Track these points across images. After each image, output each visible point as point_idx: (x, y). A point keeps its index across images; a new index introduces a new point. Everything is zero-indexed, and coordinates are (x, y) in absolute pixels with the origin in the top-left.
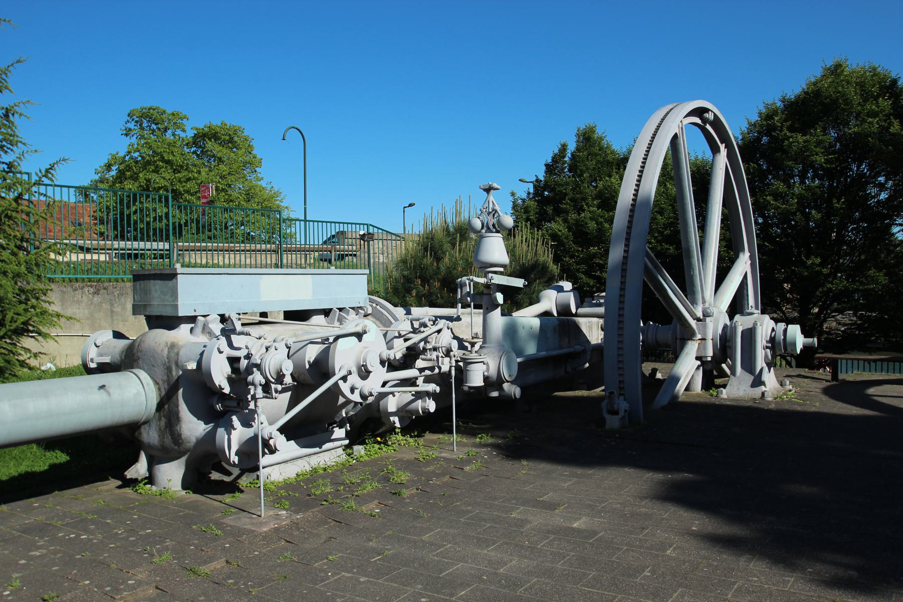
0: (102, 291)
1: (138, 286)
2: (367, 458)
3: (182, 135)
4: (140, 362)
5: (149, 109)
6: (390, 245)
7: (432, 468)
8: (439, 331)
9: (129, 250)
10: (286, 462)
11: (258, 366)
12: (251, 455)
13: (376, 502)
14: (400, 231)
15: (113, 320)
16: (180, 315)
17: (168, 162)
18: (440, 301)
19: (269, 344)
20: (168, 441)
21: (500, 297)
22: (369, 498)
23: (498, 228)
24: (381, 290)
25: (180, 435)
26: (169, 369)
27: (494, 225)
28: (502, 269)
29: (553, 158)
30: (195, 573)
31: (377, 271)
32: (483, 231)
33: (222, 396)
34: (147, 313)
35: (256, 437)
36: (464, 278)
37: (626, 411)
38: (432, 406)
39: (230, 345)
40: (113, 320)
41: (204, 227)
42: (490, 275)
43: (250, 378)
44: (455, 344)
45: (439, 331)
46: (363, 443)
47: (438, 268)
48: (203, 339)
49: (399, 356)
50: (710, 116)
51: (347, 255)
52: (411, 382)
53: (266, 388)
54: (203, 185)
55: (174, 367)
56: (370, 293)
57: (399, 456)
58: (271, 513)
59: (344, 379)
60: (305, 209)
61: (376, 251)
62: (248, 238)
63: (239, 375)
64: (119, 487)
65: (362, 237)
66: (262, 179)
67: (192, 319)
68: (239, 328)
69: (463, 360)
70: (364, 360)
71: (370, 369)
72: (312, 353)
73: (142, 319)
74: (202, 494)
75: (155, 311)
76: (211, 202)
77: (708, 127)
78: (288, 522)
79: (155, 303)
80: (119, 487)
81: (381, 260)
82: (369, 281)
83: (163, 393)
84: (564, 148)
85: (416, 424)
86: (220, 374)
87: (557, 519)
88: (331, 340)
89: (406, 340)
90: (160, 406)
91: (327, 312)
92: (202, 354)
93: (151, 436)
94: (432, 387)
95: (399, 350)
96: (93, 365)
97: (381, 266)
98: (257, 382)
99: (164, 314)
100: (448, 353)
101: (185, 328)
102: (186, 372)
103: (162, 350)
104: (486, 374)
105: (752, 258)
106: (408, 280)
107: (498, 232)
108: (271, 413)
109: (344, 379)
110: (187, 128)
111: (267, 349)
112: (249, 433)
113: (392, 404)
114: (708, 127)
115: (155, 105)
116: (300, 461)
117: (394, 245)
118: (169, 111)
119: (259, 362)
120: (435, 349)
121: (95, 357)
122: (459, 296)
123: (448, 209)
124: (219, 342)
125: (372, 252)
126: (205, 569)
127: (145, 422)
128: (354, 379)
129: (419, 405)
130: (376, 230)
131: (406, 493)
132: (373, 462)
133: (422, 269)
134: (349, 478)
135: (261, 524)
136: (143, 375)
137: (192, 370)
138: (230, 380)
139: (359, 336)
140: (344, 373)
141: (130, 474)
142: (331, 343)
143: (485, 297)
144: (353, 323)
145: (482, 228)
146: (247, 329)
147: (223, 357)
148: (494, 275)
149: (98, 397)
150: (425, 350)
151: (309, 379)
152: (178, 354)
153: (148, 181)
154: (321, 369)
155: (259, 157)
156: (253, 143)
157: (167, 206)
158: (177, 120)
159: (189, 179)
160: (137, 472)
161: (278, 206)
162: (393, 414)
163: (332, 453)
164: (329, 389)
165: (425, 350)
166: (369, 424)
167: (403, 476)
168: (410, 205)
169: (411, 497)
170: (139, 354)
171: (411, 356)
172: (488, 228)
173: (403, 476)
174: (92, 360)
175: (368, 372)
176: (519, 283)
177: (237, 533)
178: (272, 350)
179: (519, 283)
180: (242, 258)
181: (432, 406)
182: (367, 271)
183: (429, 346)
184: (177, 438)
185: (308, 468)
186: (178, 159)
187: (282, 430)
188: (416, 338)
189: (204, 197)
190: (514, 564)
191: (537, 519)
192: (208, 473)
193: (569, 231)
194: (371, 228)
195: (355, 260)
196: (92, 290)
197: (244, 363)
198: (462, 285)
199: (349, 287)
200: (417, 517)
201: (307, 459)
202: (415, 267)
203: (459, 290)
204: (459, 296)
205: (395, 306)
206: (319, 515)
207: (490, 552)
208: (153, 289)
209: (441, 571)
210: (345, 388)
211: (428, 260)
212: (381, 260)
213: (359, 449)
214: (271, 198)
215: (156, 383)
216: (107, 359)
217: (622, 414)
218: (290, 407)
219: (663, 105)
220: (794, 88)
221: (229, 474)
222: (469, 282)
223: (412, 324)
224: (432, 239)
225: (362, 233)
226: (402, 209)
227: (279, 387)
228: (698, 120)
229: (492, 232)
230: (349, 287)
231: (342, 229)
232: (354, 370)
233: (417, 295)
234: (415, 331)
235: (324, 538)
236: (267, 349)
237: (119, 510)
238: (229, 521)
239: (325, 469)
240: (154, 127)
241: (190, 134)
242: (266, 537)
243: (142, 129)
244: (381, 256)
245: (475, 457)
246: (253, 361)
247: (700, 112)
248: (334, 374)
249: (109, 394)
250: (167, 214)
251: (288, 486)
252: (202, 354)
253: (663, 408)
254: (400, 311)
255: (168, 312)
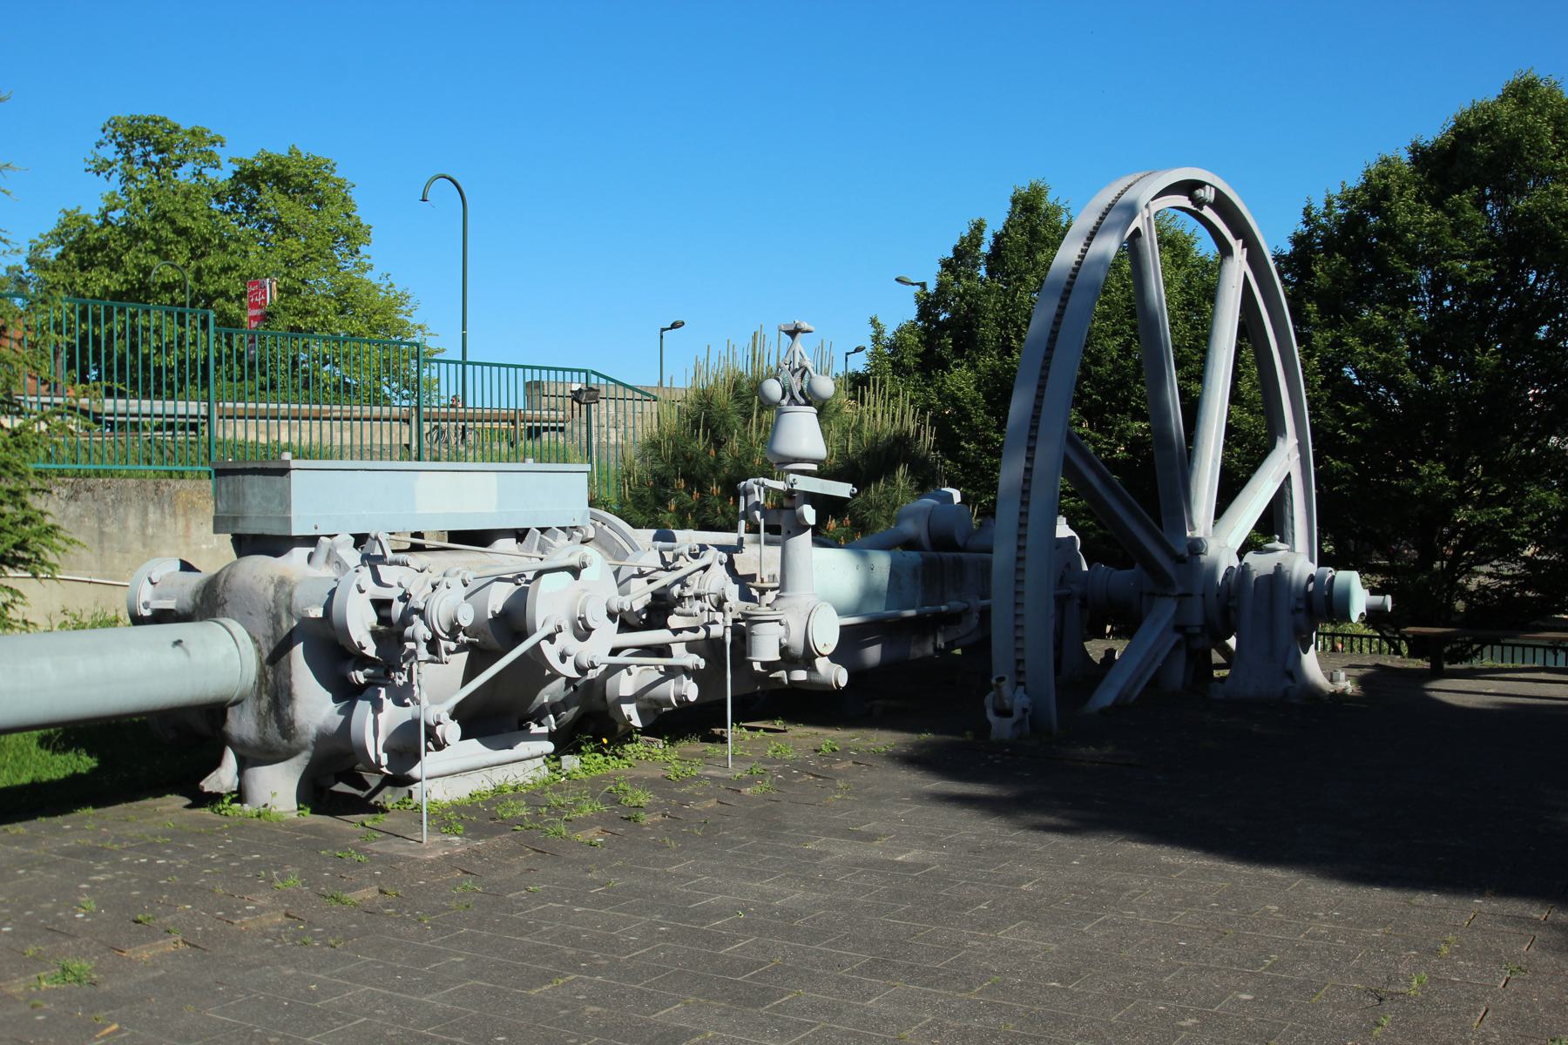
0: (84, 494)
1: (223, 488)
2: (583, 775)
3: (211, 174)
4: (228, 607)
5: (146, 121)
6: (629, 410)
7: (688, 789)
8: (706, 568)
9: (133, 415)
10: (457, 769)
11: (421, 613)
12: (409, 744)
13: (598, 828)
14: (648, 380)
15: (102, 548)
16: (294, 533)
17: (182, 232)
18: (720, 520)
19: (436, 580)
20: (273, 732)
21: (809, 514)
22: (587, 823)
23: (809, 397)
24: (612, 498)
25: (292, 723)
26: (276, 619)
27: (801, 393)
28: (814, 467)
29: (956, 250)
30: (337, 900)
31: (604, 461)
32: (785, 402)
33: (363, 661)
34: (238, 531)
35: (415, 722)
36: (751, 481)
37: (1025, 710)
38: (691, 691)
39: (377, 579)
40: (102, 548)
41: (251, 365)
42: (792, 476)
43: (408, 631)
44: (732, 591)
45: (706, 568)
46: (577, 751)
47: (719, 459)
48: (329, 572)
49: (638, 606)
50: (1208, 194)
51: (546, 429)
52: (663, 650)
53: (433, 646)
54: (252, 278)
55: (284, 616)
56: (592, 503)
57: (636, 773)
58: (437, 839)
59: (551, 638)
60: (464, 336)
61: (604, 421)
62: (344, 390)
63: (391, 632)
64: (188, 807)
65: (576, 396)
66: (370, 267)
67: (312, 541)
68: (390, 556)
69: (746, 617)
70: (585, 598)
71: (591, 624)
72: (497, 598)
73: (227, 538)
74: (332, 814)
75: (252, 527)
76: (268, 317)
77: (1207, 212)
78: (464, 849)
79: (253, 513)
80: (188, 807)
81: (613, 441)
82: (590, 481)
83: (266, 655)
84: (979, 227)
85: (671, 723)
86: (360, 626)
87: (875, 851)
88: (530, 576)
89: (650, 582)
90: (262, 675)
91: (520, 535)
92: (332, 593)
93: (243, 724)
94: (695, 661)
95: (639, 597)
96: (147, 613)
97: (612, 452)
98: (419, 636)
99: (268, 532)
100: (720, 604)
101: (300, 553)
102: (306, 622)
103: (265, 589)
104: (784, 641)
105: (1302, 447)
106: (662, 481)
107: (808, 404)
108: (440, 685)
109: (551, 638)
110: (224, 162)
111: (434, 588)
112: (405, 714)
113: (625, 685)
114: (1207, 212)
115: (159, 114)
116: (475, 775)
117: (638, 409)
118: (186, 126)
119: (422, 606)
120: (698, 597)
121: (148, 600)
122: (742, 508)
123: (738, 351)
124: (359, 576)
125: (594, 423)
126: (354, 897)
127: (237, 702)
128: (566, 640)
129: (670, 689)
130: (603, 381)
131: (645, 819)
132: (596, 782)
133: (688, 460)
134: (554, 798)
135: (424, 851)
136: (236, 627)
137: (317, 619)
138: (375, 634)
139: (575, 571)
140: (549, 629)
141: (209, 784)
142: (528, 582)
143: (785, 513)
144: (564, 551)
145: (783, 397)
146: (402, 557)
147: (366, 597)
148: (798, 477)
149: (174, 657)
150: (681, 598)
151: (493, 642)
152: (290, 595)
153: (146, 271)
154: (511, 624)
155: (364, 222)
156: (354, 195)
157: (182, 325)
158: (201, 143)
159: (226, 270)
160: (219, 782)
161: (402, 325)
162: (628, 700)
163: (527, 760)
164: (524, 656)
165: (681, 598)
166: (590, 721)
167: (644, 798)
168: (674, 326)
169: (654, 824)
170: (227, 596)
171: (660, 609)
172: (793, 397)
173: (644, 798)
174: (146, 605)
175: (589, 630)
176: (843, 490)
177: (390, 861)
178: (442, 588)
179: (843, 490)
180: (340, 435)
181: (691, 691)
182: (588, 467)
183: (688, 592)
184: (287, 727)
185: (490, 788)
186: (201, 226)
187: (456, 714)
188: (665, 578)
189: (254, 305)
190: (797, 895)
191: (843, 850)
192: (337, 779)
193: (978, 389)
194: (594, 379)
195: (561, 439)
196: (65, 492)
197: (397, 609)
198: (747, 493)
199: (556, 494)
200: (660, 847)
201: (486, 772)
202: (675, 457)
203: (742, 499)
204: (742, 508)
205: (635, 526)
206: (511, 843)
207: (767, 886)
208: (249, 492)
209: (691, 902)
210: (551, 652)
211: (700, 444)
212: (613, 441)
213: (570, 762)
214: (389, 308)
215: (255, 640)
216: (170, 604)
217: (1017, 715)
218: (469, 676)
219: (1118, 177)
220: (1433, 129)
221: (363, 785)
222: (757, 489)
223: (662, 557)
224: (709, 405)
225: (576, 387)
226: (655, 348)
227: (453, 646)
228: (1184, 201)
229: (798, 404)
230: (556, 494)
231: (536, 378)
232: (566, 625)
233: (677, 508)
234: (667, 567)
235: (518, 870)
236: (434, 588)
237: (199, 834)
238: (375, 847)
239: (515, 789)
240: (154, 158)
241: (222, 175)
242: (433, 865)
243: (130, 160)
244: (613, 432)
245: (762, 776)
246: (412, 604)
247: (1188, 188)
248: (535, 631)
249: (188, 653)
250: (182, 337)
251: (457, 807)
252: (332, 593)
253: (1103, 711)
254: (646, 535)
255: (274, 529)
